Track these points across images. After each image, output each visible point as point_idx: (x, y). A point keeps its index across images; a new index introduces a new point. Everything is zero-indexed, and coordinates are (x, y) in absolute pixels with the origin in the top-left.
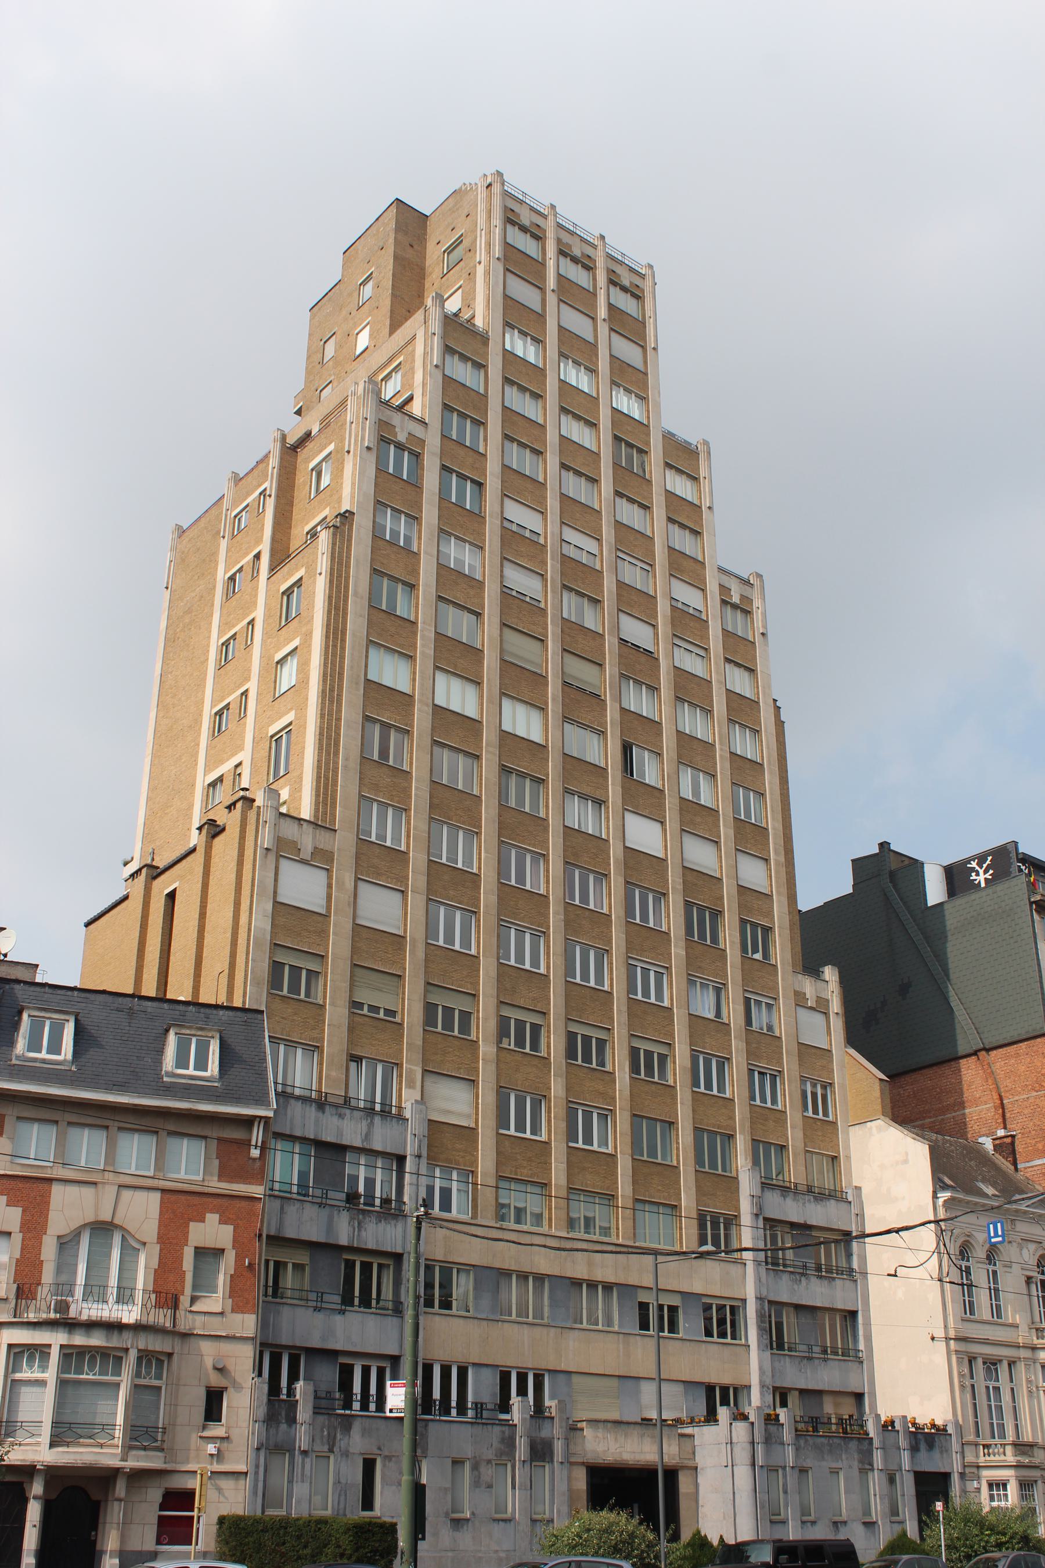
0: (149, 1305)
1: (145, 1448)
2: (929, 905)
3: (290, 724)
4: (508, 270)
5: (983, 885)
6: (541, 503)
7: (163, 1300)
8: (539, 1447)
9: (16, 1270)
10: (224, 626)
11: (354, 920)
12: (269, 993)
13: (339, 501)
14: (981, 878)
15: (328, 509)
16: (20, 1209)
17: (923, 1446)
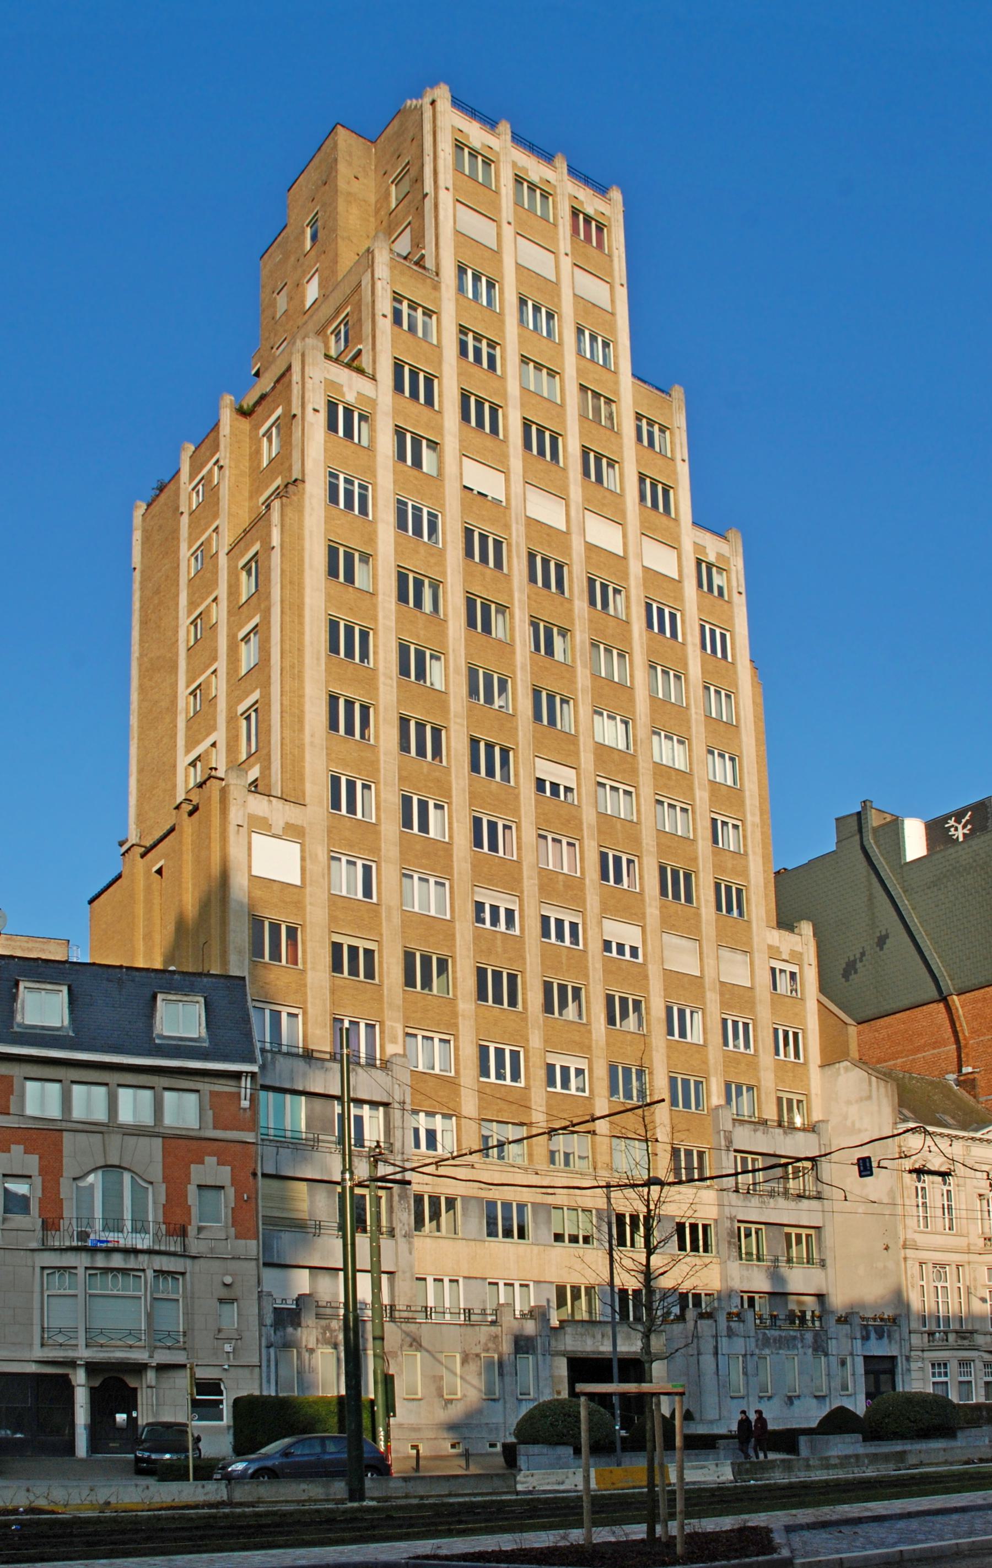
0: (160, 1234)
1: (169, 1348)
2: (909, 859)
3: (256, 702)
4: (458, 201)
5: (961, 839)
6: (502, 462)
7: (172, 1230)
8: (522, 1343)
9: (40, 1207)
10: (192, 605)
11: (329, 889)
12: (251, 960)
13: (290, 469)
14: (960, 834)
15: (280, 478)
16: (37, 1157)
17: (873, 1335)
